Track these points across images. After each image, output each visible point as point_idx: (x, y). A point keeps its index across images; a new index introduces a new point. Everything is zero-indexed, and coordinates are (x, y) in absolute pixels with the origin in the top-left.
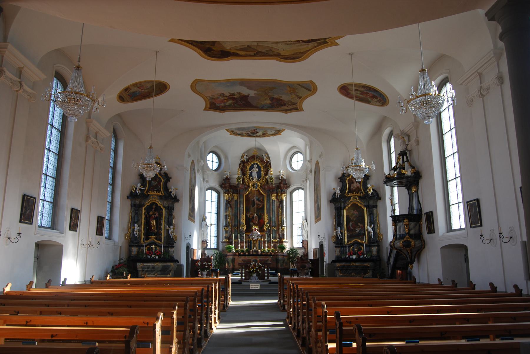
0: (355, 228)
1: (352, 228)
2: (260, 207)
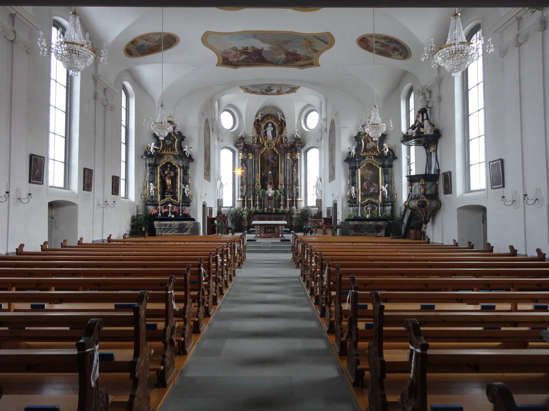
0: (369, 187)
1: (366, 188)
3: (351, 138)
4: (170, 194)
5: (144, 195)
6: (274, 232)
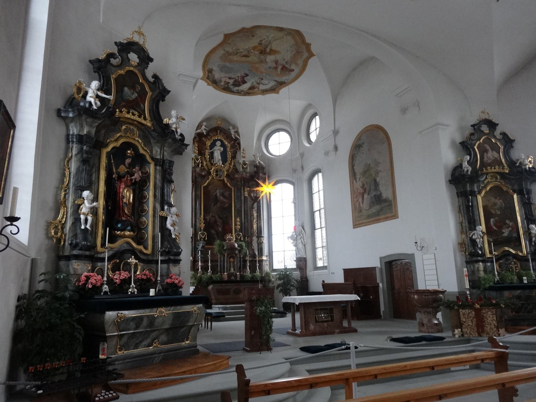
0: (500, 227)
1: (495, 228)
2: (226, 206)
3: (453, 143)
4: (129, 228)
5: (56, 227)
6: (332, 320)
